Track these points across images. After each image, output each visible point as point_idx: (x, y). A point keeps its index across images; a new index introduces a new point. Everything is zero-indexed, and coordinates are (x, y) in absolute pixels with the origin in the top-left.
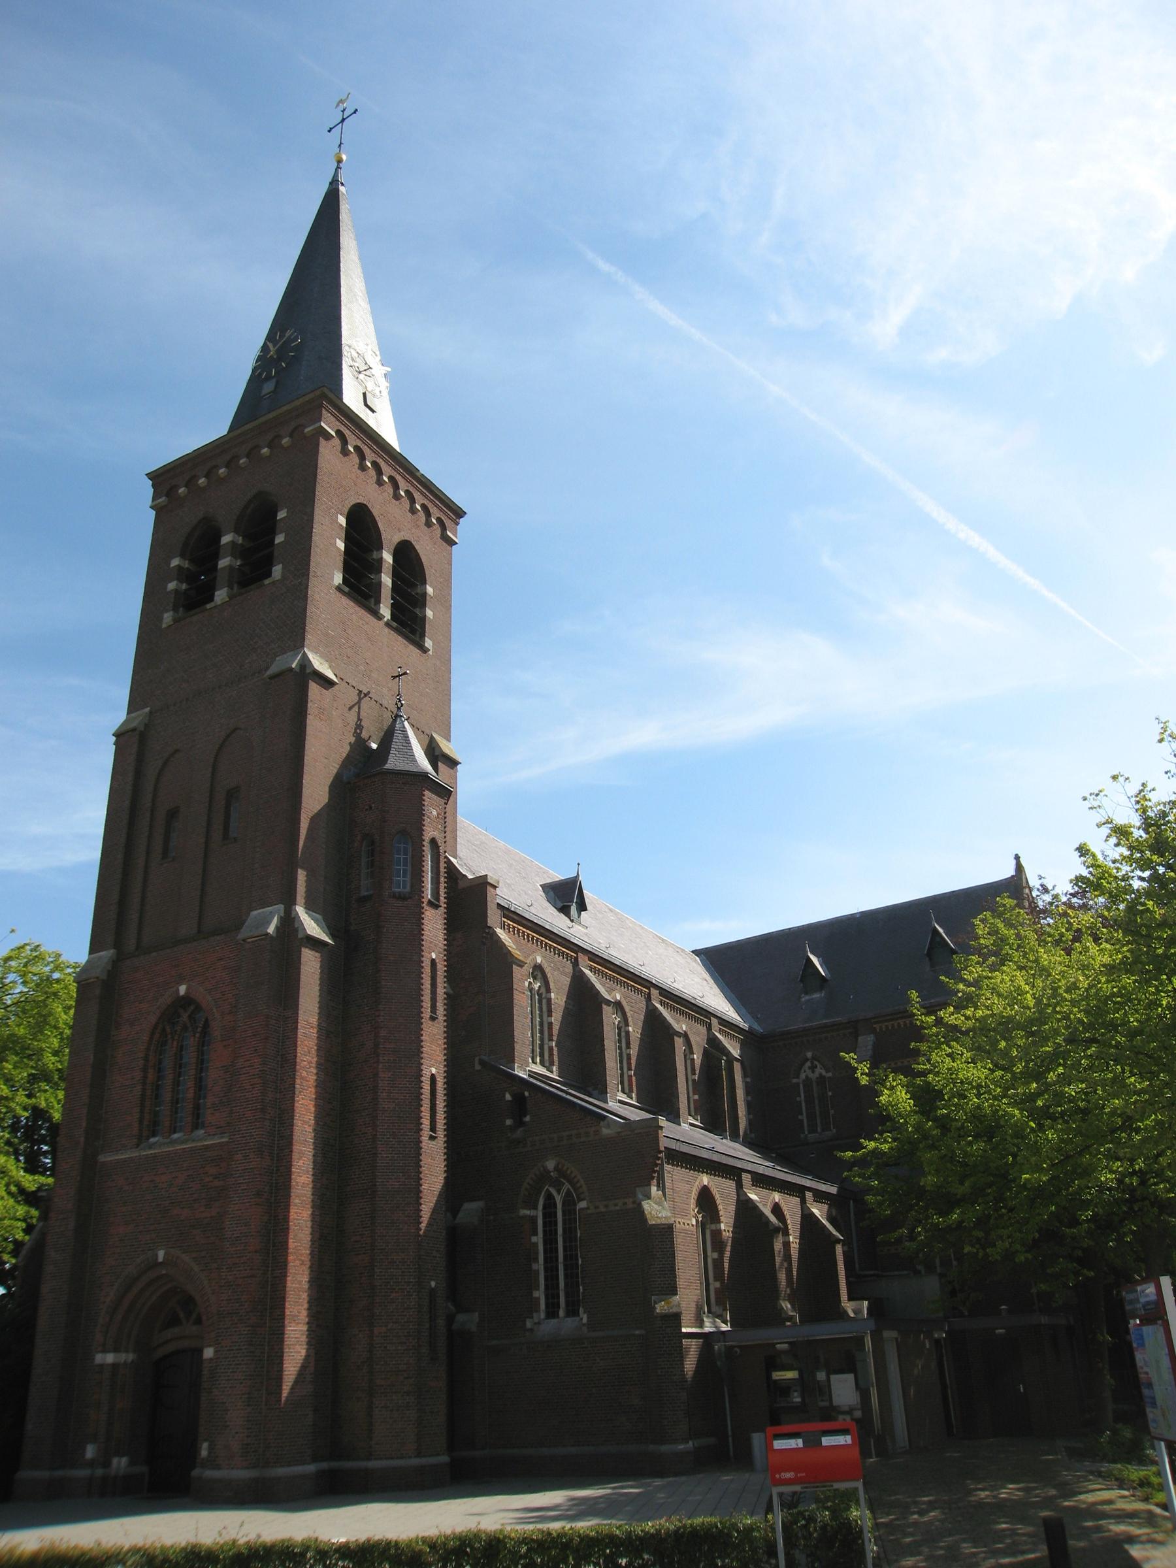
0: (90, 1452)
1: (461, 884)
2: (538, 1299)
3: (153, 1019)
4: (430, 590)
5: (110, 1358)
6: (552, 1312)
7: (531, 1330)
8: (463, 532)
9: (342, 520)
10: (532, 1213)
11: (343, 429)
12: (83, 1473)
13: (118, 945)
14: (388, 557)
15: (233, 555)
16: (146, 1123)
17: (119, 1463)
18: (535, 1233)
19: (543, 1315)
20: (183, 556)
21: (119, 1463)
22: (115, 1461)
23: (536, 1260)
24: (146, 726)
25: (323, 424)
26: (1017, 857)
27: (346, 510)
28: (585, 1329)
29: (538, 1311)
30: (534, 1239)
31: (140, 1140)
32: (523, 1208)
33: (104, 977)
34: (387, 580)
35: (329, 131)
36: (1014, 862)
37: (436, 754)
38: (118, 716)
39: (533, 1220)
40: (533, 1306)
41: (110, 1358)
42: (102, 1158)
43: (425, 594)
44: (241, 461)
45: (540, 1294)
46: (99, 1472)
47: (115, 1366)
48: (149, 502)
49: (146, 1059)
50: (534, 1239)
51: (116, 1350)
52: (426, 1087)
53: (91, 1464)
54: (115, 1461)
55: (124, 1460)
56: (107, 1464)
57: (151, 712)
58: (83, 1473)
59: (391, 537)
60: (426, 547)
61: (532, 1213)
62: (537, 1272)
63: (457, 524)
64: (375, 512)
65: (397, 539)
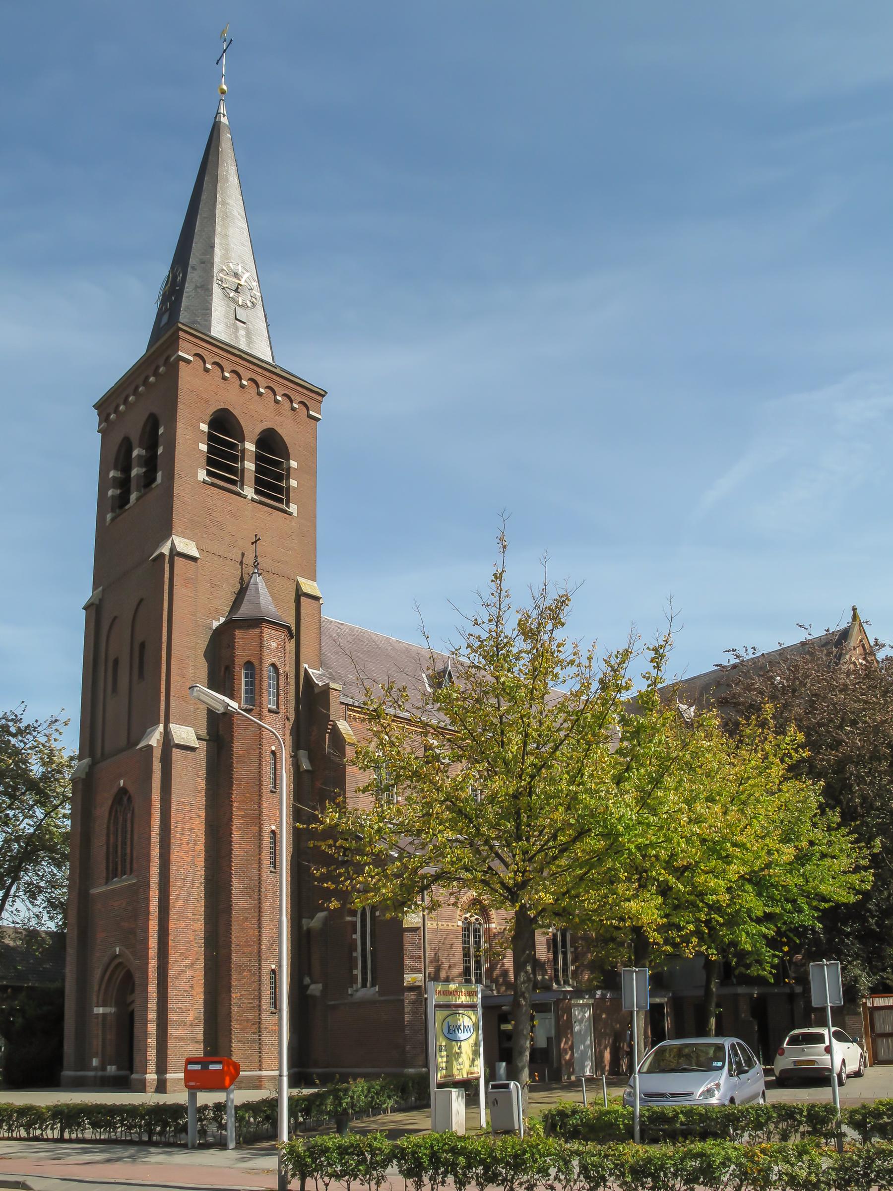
0: (95, 1062)
1: (316, 690)
2: (357, 975)
3: (110, 802)
4: (294, 464)
5: (101, 1010)
6: (364, 985)
7: (352, 995)
8: (326, 409)
9: (204, 427)
10: (354, 919)
11: (200, 351)
12: (91, 1074)
13: (92, 754)
14: (250, 447)
15: (140, 466)
16: (111, 868)
17: (111, 1068)
18: (355, 933)
19: (359, 986)
20: (116, 468)
21: (111, 1068)
22: (109, 1067)
23: (356, 950)
24: (101, 600)
25: (180, 353)
26: (854, 609)
27: (208, 419)
28: (377, 995)
29: (356, 983)
30: (354, 936)
31: (107, 881)
32: (348, 916)
33: (84, 776)
34: (250, 465)
35: (217, 63)
36: (851, 613)
37: (300, 593)
38: (86, 593)
39: (354, 924)
40: (353, 980)
41: (101, 1010)
42: (94, 891)
43: (289, 469)
44: (140, 389)
45: (358, 972)
46: (100, 1073)
47: (104, 1015)
48: (97, 428)
49: (108, 828)
50: (354, 936)
51: (104, 1006)
52: (267, 839)
53: (96, 1069)
54: (109, 1067)
55: (114, 1067)
56: (104, 1069)
57: (103, 590)
58: (91, 1074)
59: (252, 429)
60: (288, 431)
61: (354, 919)
62: (356, 957)
63: (321, 402)
64: (236, 412)
65: (258, 430)
